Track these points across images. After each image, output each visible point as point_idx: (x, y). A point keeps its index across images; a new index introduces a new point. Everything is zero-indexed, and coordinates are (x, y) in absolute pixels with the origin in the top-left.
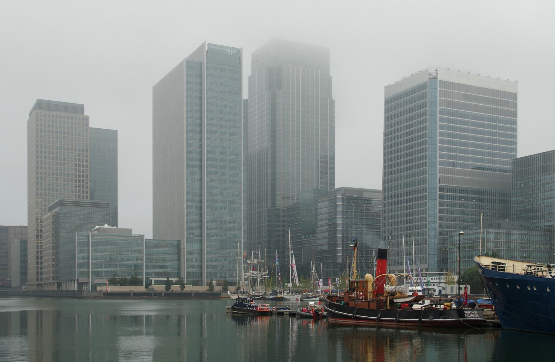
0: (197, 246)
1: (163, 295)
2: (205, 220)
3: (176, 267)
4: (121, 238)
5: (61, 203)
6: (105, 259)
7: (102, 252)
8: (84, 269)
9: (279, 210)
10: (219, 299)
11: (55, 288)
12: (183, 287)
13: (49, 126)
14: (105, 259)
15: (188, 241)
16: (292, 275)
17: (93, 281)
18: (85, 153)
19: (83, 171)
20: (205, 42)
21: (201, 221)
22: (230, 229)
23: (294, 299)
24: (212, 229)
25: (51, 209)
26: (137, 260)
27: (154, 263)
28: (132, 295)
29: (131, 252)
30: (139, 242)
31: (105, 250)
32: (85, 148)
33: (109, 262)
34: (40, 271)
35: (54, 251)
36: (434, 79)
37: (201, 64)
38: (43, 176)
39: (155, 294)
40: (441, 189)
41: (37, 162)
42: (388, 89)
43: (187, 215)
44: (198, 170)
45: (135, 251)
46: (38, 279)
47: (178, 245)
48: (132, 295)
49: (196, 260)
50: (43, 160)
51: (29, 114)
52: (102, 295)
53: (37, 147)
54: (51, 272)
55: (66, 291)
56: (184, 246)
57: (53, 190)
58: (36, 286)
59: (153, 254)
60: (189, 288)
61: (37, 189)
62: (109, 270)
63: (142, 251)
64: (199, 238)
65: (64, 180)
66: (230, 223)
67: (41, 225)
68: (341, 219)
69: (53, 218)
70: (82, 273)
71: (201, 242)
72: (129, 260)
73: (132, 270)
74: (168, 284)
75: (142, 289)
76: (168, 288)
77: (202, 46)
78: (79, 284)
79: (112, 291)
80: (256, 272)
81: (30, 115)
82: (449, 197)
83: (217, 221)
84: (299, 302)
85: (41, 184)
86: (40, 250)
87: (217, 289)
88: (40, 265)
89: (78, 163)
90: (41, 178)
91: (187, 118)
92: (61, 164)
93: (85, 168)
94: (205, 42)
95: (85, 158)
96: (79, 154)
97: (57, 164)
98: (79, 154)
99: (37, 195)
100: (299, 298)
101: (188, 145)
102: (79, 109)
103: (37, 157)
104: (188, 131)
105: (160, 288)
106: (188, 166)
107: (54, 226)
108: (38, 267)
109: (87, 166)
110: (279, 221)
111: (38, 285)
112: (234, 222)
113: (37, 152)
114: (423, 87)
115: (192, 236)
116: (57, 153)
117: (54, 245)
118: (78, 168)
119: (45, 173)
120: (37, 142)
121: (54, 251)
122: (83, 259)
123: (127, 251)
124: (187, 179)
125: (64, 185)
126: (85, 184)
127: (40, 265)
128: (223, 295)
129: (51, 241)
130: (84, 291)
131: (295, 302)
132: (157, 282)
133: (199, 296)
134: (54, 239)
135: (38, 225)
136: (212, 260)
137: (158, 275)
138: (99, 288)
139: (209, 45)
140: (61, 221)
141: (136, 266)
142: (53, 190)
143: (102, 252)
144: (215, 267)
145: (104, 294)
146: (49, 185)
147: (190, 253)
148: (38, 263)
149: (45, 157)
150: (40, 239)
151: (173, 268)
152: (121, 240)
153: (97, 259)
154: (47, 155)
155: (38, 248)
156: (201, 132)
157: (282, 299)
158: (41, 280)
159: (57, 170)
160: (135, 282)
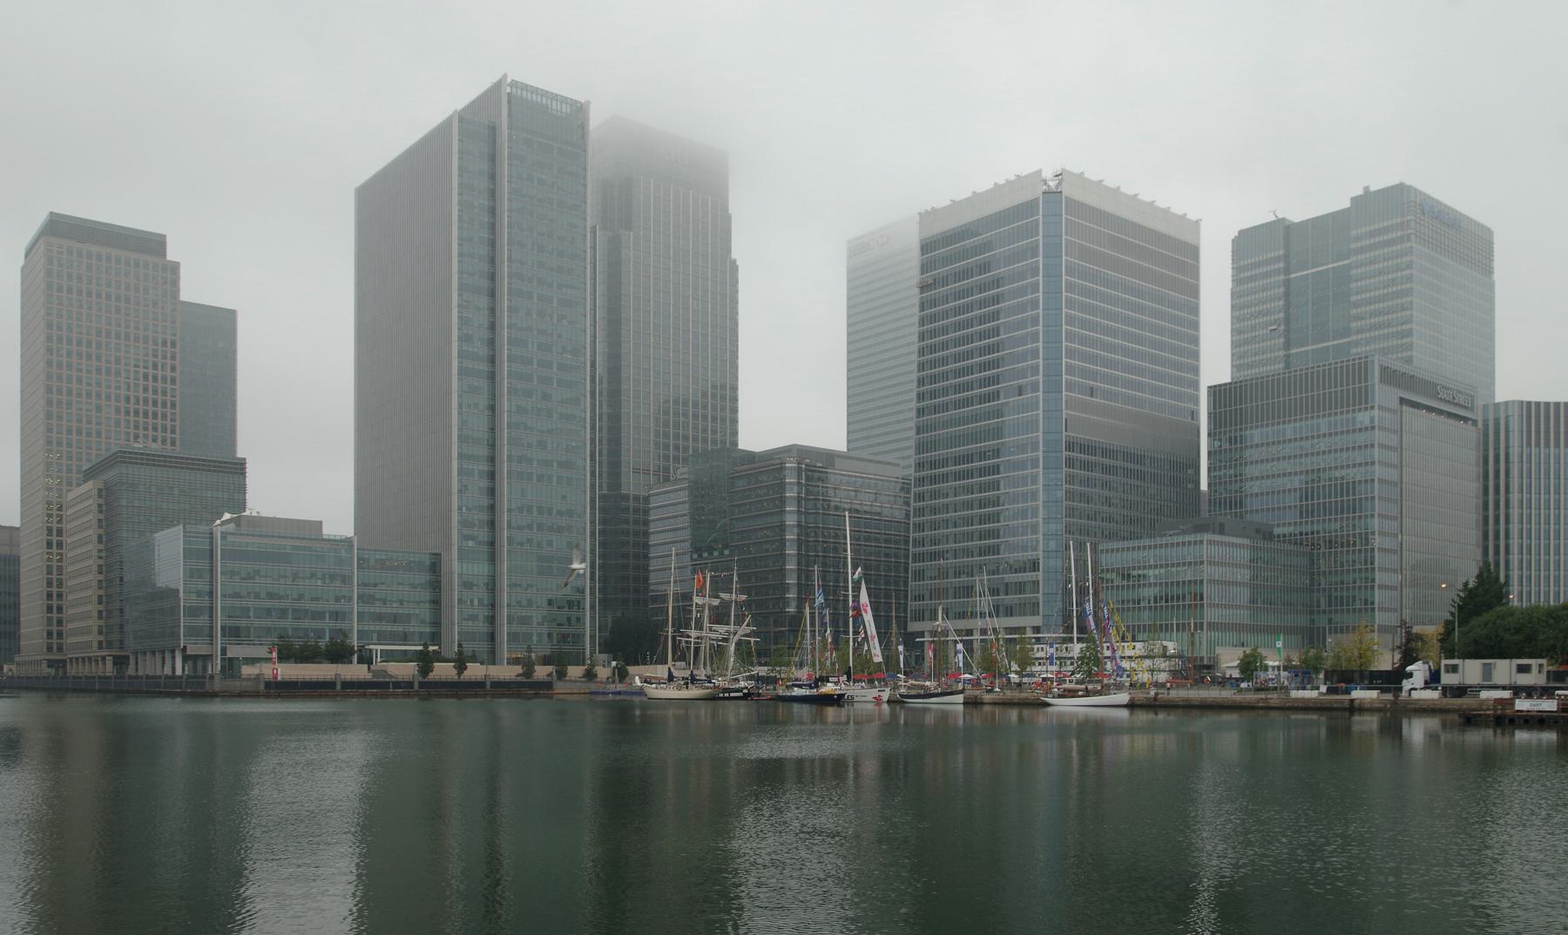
0: (480, 569)
1: (416, 686)
2: (505, 503)
3: (427, 616)
4: (298, 543)
5: (122, 458)
6: (257, 596)
7: (249, 577)
8: (203, 620)
9: (626, 497)
10: (550, 697)
11: (109, 668)
12: (461, 667)
13: (80, 279)
14: (257, 596)
15: (463, 555)
16: (856, 633)
17: (224, 651)
18: (169, 349)
19: (164, 393)
20: (505, 76)
21: (492, 508)
22: (560, 529)
23: (870, 698)
24: (519, 528)
25: (89, 475)
26: (337, 599)
27: (377, 608)
28: (339, 687)
29: (323, 578)
30: (343, 554)
31: (257, 572)
32: (169, 338)
33: (269, 604)
34: (55, 629)
35: (101, 577)
36: (1052, 196)
37: (493, 130)
38: (64, 398)
39: (397, 685)
40: (1070, 446)
41: (49, 363)
42: (856, 249)
43: (460, 491)
44: (483, 384)
45: (333, 577)
46: (50, 649)
47: (435, 567)
48: (339, 687)
49: (480, 600)
50: (65, 360)
51: (23, 252)
52: (262, 687)
53: (50, 326)
54: (95, 629)
55: (148, 677)
56: (455, 567)
57: (89, 434)
58: (44, 665)
59: (375, 585)
60: (475, 671)
61: (50, 430)
62: (268, 623)
63: (351, 578)
64: (485, 548)
65: (118, 411)
66: (560, 513)
67: (60, 516)
68: (795, 517)
69: (100, 496)
70: (193, 632)
71: (493, 558)
72: (317, 599)
73: (327, 624)
74: (425, 661)
75: (355, 671)
76: (425, 669)
77: (497, 86)
78: (186, 658)
79: (287, 678)
80: (725, 628)
81: (27, 256)
82: (1087, 466)
83: (530, 510)
84: (885, 706)
85: (60, 418)
86: (55, 577)
87: (542, 672)
88: (55, 615)
89: (151, 372)
90: (60, 403)
91: (460, 255)
92: (108, 372)
93: (169, 386)
94: (505, 76)
95: (169, 362)
96: (155, 350)
97: (99, 371)
98: (155, 350)
99: (49, 443)
100: (885, 696)
101: (463, 321)
102: (153, 245)
103: (50, 350)
104: (462, 288)
105: (406, 670)
106: (462, 372)
107: (102, 516)
108: (50, 620)
109: (173, 381)
110: (627, 521)
111: (51, 664)
112: (570, 513)
113: (49, 338)
114: (1029, 208)
115: (471, 543)
116: (99, 345)
117: (101, 562)
118: (151, 383)
119: (69, 392)
120: (49, 314)
121: (101, 577)
122: (199, 594)
123: (313, 575)
124: (460, 406)
125: (118, 424)
126: (169, 423)
127: (55, 615)
128: (560, 687)
129: (95, 553)
130: (212, 677)
131: (870, 706)
132: (389, 656)
133: (502, 688)
134: (102, 547)
135: (49, 516)
136: (519, 603)
137: (383, 637)
138: (247, 670)
139: (514, 84)
140: (124, 502)
141: (336, 616)
142: (89, 434)
143: (249, 577)
144: (525, 621)
145: (268, 685)
146: (79, 421)
147: (467, 585)
148: (50, 609)
149: (69, 354)
150: (55, 550)
151: (423, 621)
152: (294, 547)
153: (237, 595)
154: (74, 348)
155: (50, 573)
156: (492, 294)
157: (836, 700)
158: (60, 649)
159: (99, 384)
160: (339, 654)
